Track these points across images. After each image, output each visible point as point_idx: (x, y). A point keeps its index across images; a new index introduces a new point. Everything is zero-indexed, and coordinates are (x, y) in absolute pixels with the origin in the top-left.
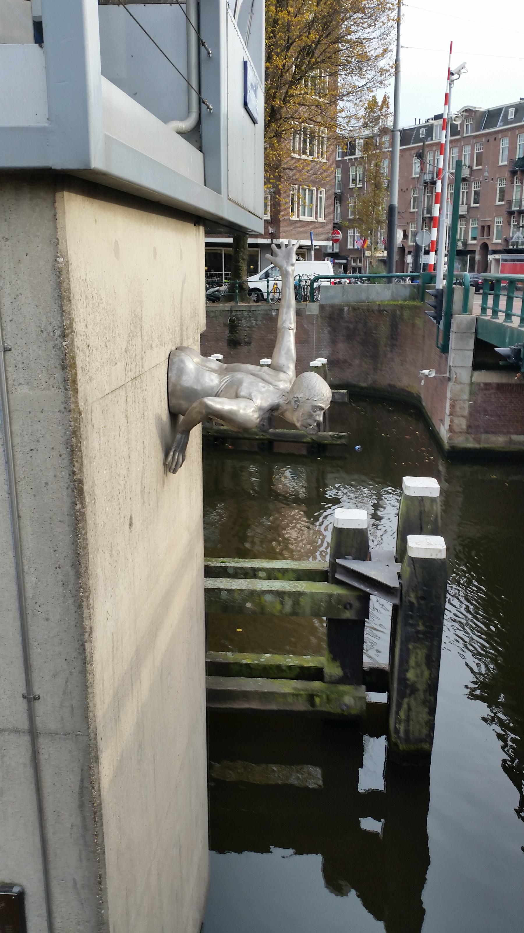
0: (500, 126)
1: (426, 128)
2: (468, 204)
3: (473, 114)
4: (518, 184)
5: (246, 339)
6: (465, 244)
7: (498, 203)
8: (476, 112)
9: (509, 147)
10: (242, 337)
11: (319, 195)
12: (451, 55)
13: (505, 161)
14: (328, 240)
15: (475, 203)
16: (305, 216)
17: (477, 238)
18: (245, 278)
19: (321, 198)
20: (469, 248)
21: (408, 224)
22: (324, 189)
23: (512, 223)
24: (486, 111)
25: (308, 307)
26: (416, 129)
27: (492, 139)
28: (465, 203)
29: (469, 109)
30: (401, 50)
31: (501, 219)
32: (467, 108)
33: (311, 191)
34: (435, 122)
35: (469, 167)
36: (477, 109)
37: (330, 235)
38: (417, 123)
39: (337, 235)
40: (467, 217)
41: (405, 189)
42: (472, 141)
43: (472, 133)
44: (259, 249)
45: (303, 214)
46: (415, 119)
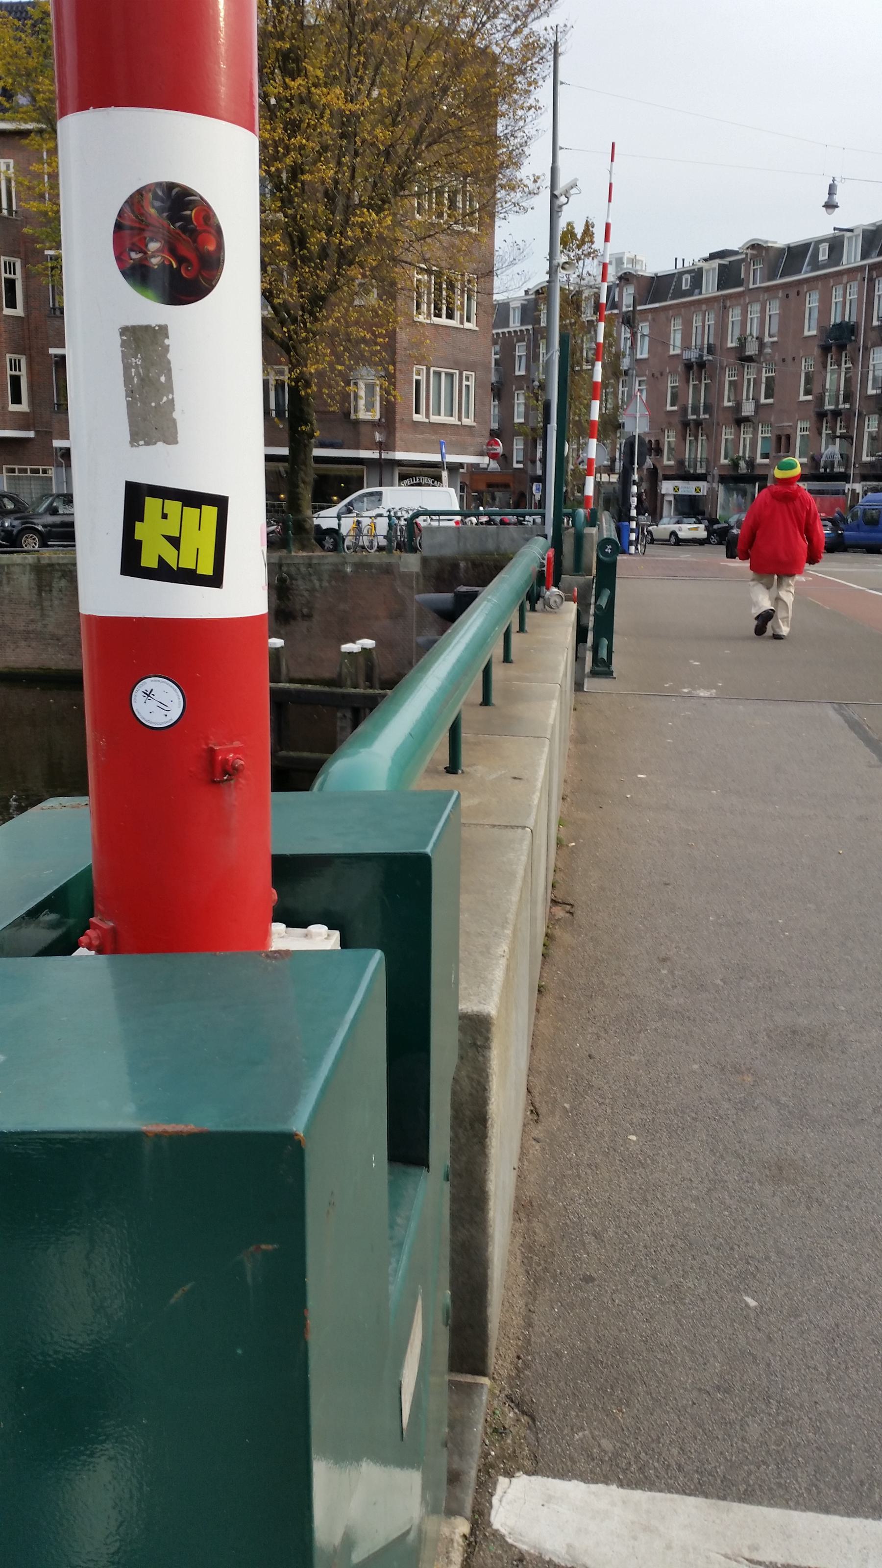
0: (806, 272)
1: (693, 274)
2: (756, 399)
3: (764, 252)
4: (833, 367)
5: (305, 611)
6: (751, 464)
7: (802, 398)
8: (768, 249)
9: (819, 306)
10: (298, 607)
11: (465, 383)
12: (613, 163)
13: (813, 330)
14: (481, 454)
15: (766, 398)
16: (439, 415)
17: (771, 456)
18: (309, 512)
19: (468, 387)
20: (759, 472)
21: (663, 431)
22: (473, 374)
23: (824, 431)
24: (784, 247)
25: (402, 560)
26: (677, 275)
27: (793, 294)
28: (751, 397)
29: (758, 244)
30: (560, 154)
31: (807, 425)
32: (753, 243)
33: (450, 376)
34: (705, 265)
35: (757, 338)
36: (770, 245)
37: (485, 447)
38: (680, 265)
39: (495, 447)
40: (754, 421)
41: (657, 374)
42: (761, 296)
43: (763, 282)
44: (365, 468)
45: (436, 412)
46: (676, 259)
